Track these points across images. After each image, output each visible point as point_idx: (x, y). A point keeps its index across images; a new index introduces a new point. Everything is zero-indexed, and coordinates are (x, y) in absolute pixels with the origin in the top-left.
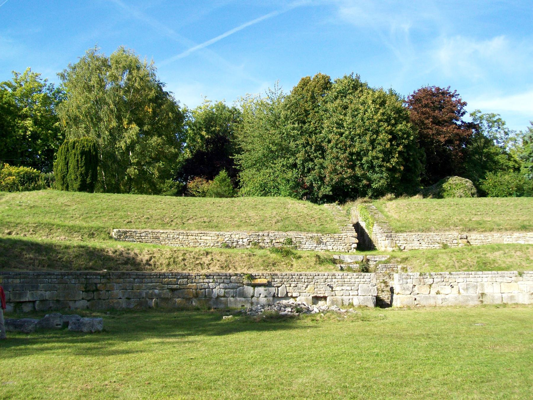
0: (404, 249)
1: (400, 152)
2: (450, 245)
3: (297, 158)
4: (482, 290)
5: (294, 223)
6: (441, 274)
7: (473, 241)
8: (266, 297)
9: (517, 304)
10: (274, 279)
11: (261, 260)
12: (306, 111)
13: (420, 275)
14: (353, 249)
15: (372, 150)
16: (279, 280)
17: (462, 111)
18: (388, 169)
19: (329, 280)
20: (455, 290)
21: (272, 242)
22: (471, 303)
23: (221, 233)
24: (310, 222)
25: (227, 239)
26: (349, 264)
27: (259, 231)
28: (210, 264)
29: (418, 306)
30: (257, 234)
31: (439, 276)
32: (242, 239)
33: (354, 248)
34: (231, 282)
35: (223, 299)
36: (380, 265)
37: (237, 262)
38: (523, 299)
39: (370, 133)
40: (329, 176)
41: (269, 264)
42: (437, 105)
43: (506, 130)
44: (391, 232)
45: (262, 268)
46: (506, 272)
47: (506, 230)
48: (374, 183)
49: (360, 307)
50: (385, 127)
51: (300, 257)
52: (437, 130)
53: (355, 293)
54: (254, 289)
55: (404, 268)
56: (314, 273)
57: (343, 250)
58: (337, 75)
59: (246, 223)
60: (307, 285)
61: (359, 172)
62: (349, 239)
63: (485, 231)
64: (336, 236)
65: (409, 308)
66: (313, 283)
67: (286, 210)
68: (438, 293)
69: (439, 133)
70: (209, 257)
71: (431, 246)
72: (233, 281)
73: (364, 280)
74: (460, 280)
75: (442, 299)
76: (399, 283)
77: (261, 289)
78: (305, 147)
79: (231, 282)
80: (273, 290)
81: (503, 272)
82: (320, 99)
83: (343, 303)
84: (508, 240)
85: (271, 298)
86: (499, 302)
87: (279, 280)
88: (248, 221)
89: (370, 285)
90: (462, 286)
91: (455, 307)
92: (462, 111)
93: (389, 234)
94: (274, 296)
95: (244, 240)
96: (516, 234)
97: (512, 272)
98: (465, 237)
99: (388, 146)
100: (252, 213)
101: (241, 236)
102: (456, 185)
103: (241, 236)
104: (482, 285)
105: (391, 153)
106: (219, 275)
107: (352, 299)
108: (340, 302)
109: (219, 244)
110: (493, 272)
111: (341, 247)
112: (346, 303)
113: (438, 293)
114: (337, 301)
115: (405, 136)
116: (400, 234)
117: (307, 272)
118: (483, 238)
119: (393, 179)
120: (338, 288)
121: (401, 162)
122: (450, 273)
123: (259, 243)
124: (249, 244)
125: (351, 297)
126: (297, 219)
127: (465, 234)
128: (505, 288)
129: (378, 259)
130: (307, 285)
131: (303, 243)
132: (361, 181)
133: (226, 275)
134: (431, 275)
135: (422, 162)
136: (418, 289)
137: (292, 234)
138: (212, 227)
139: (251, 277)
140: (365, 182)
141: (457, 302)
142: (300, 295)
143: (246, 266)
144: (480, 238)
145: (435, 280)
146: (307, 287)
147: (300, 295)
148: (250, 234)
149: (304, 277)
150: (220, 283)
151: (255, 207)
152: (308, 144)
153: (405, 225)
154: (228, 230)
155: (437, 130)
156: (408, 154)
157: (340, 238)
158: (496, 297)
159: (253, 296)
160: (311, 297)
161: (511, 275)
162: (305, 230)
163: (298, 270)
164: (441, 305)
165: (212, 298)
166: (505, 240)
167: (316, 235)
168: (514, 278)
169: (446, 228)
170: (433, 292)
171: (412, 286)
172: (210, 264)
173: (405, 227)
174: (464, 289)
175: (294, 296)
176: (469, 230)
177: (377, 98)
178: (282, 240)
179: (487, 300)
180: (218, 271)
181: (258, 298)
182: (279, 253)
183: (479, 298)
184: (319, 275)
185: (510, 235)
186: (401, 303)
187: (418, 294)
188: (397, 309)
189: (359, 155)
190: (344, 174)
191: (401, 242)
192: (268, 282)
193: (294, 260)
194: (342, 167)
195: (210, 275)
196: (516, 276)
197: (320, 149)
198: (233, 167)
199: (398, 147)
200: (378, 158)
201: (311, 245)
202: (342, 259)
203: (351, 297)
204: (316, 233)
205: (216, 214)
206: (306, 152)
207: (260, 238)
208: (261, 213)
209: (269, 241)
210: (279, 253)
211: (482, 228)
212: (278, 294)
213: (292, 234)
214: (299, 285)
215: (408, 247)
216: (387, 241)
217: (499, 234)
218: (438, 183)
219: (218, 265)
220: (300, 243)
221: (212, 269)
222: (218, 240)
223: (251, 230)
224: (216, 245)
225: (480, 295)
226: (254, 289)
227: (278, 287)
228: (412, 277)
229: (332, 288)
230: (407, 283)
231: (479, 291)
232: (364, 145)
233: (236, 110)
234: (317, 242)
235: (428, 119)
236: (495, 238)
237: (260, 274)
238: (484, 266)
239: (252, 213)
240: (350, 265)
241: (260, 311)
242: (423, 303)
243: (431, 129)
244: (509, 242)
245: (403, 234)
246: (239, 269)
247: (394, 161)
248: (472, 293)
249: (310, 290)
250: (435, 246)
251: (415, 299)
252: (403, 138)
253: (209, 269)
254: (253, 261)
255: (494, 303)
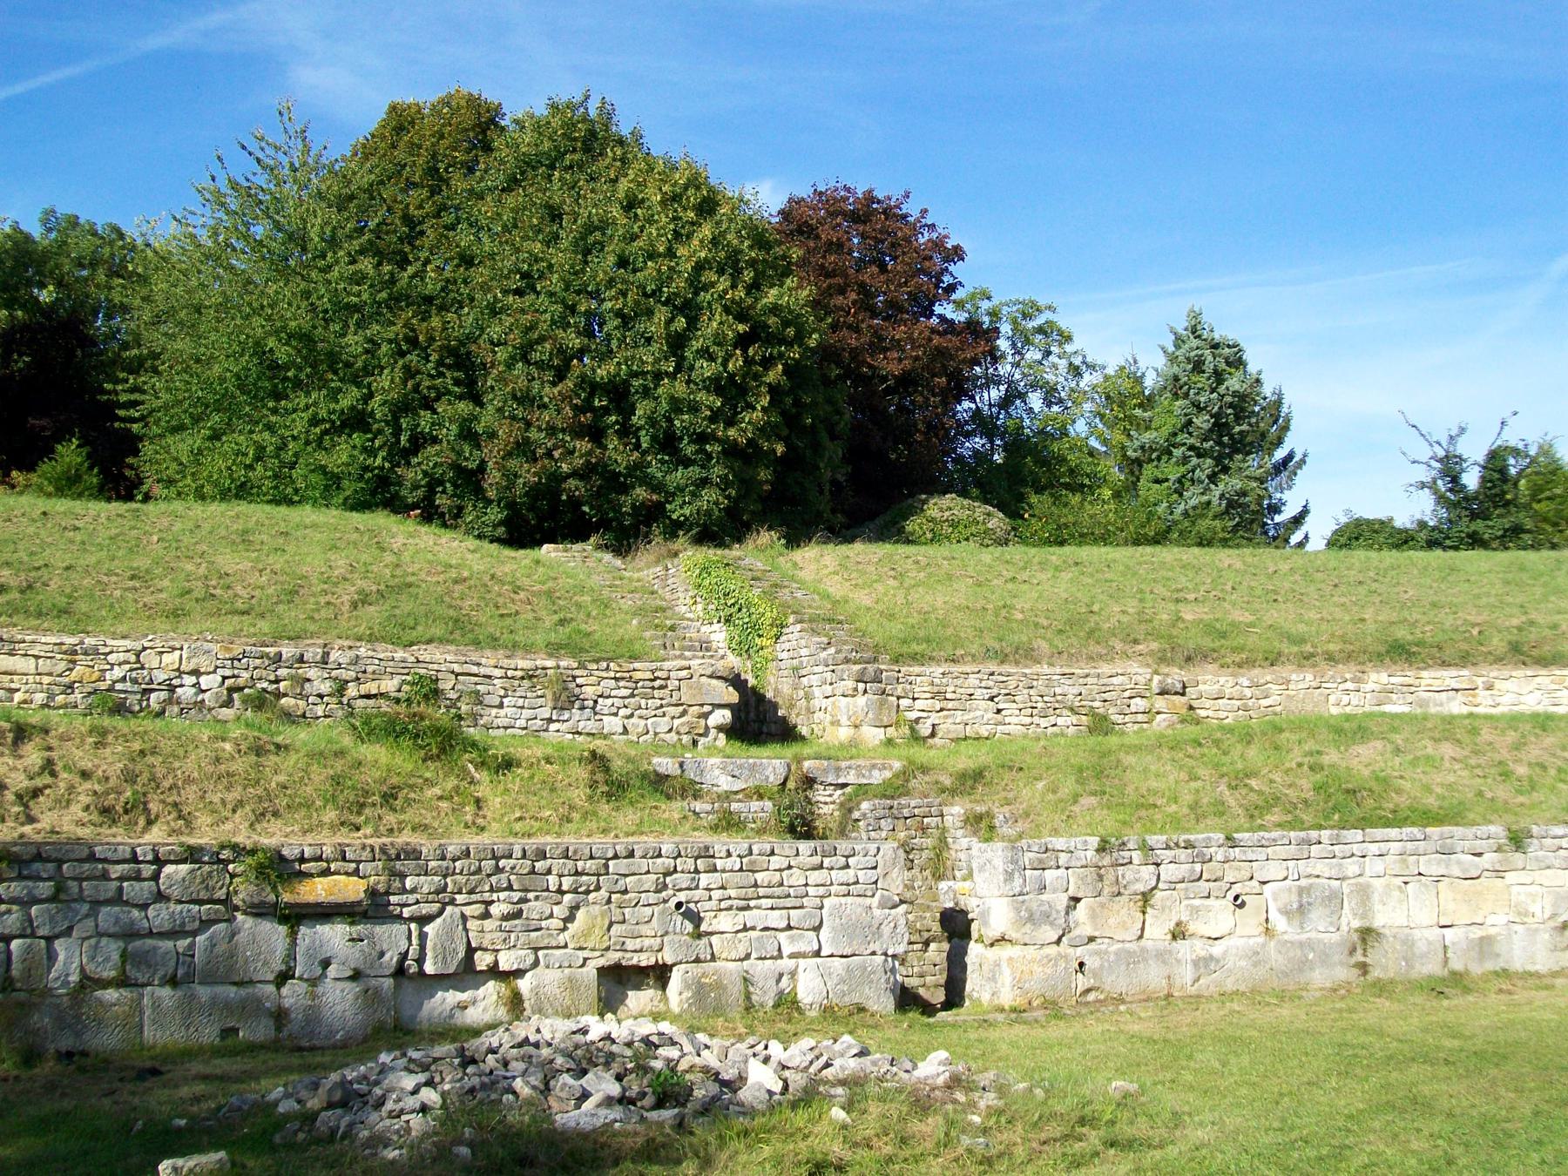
0: (933, 735)
1: (773, 390)
2: (1119, 719)
3: (371, 395)
4: (1364, 916)
5: (440, 610)
6: (1189, 845)
7: (1208, 704)
8: (356, 976)
9: (1505, 973)
10: (403, 876)
11: (319, 774)
12: (407, 219)
13: (1101, 849)
14: (713, 732)
15: (672, 376)
16: (427, 884)
17: (947, 279)
18: (732, 451)
19: (682, 879)
20: (1249, 922)
21: (341, 689)
22: (1319, 978)
23: (90, 641)
24: (514, 608)
25: (118, 672)
26: (728, 796)
27: (276, 639)
28: (36, 793)
29: (1091, 997)
30: (272, 650)
31: (1183, 854)
32: (196, 673)
33: (720, 728)
34: (161, 897)
35: (111, 994)
36: (865, 806)
37: (189, 780)
38: (1530, 951)
39: (662, 314)
40: (501, 467)
41: (366, 793)
42: (867, 254)
43: (1077, 361)
44: (876, 662)
45: (330, 815)
46: (1458, 831)
47: (1331, 658)
48: (679, 501)
49: (828, 1011)
50: (725, 292)
51: (508, 764)
52: (876, 333)
53: (807, 942)
54: (293, 934)
55: (979, 818)
56: (602, 843)
57: (673, 737)
58: (524, 97)
59: (211, 600)
60: (575, 908)
61: (618, 454)
62: (700, 687)
63: (1249, 663)
64: (642, 670)
65: (1052, 1008)
66: (603, 893)
67: (389, 558)
68: (1178, 934)
69: (878, 344)
70: (33, 755)
71: (1044, 723)
72: (175, 892)
73: (849, 875)
74: (1274, 870)
75: (1196, 963)
76: (1006, 889)
77: (334, 935)
78: (402, 354)
79: (161, 897)
80: (393, 939)
81: (1446, 829)
82: (459, 183)
83: (748, 996)
84: (1345, 699)
85: (388, 983)
86: (1431, 967)
87: (427, 884)
88: (218, 592)
89: (875, 901)
90: (1275, 897)
91: (1254, 996)
92: (947, 279)
93: (871, 668)
94: (400, 971)
95: (205, 681)
96: (1378, 678)
97: (1483, 830)
98: (1179, 687)
99: (736, 363)
100: (229, 561)
101: (193, 659)
102: (954, 524)
103: (193, 659)
104: (1364, 893)
105: (743, 391)
106: (92, 857)
107: (793, 974)
108: (736, 990)
109: (77, 696)
110: (1408, 831)
111: (663, 725)
112: (765, 996)
113: (1178, 934)
114: (719, 986)
115: (791, 331)
116: (917, 669)
117: (569, 840)
118: (1248, 693)
119: (747, 485)
120: (725, 922)
121: (776, 426)
122: (1228, 838)
123: (279, 695)
124: (228, 703)
125: (786, 964)
126: (449, 593)
127: (1175, 676)
128: (1452, 902)
129: (851, 778)
130: (575, 908)
131: (487, 700)
132: (625, 489)
133: (134, 859)
134: (1146, 848)
135: (833, 437)
136: (1093, 916)
137: (439, 659)
138: (39, 615)
139: (280, 868)
140: (641, 493)
141: (1261, 972)
142: (536, 963)
143: (240, 804)
144: (1235, 692)
145: (1168, 872)
146: (570, 918)
147: (536, 963)
148: (237, 650)
149: (557, 865)
150: (97, 904)
151: (245, 539)
152: (413, 342)
153: (922, 634)
154: (121, 629)
155: (876, 333)
156: (797, 403)
157: (658, 682)
158: (1421, 947)
159: (283, 977)
160: (590, 971)
161: (1479, 845)
162: (494, 642)
163: (518, 827)
164: (1193, 990)
165: (48, 992)
166: (1332, 699)
167: (550, 663)
168: (1489, 859)
169: (1095, 649)
170: (1157, 930)
171: (1062, 900)
172: (36, 793)
173: (928, 641)
174: (1286, 912)
175: (504, 966)
176: (1189, 659)
177: (686, 187)
178: (389, 685)
179: (1385, 964)
180: (85, 832)
181: (314, 982)
182: (406, 742)
183: (1353, 951)
184: (631, 855)
185: (1355, 680)
186: (1018, 985)
187: (1091, 939)
188: (1000, 1017)
189: (619, 395)
190: (561, 459)
191: (919, 704)
192: (372, 893)
193: (482, 776)
194: (552, 430)
195: (38, 857)
196: (1499, 850)
197: (465, 368)
198: (116, 425)
199: (766, 369)
200: (694, 408)
201: (527, 713)
202: (691, 774)
203: (786, 964)
204: (551, 655)
205: (60, 559)
206: (409, 373)
207: (282, 672)
208: (277, 562)
209: (325, 688)
210: (406, 742)
211: (1234, 650)
212: (420, 960)
213: (438, 657)
214: (534, 908)
215: (949, 726)
216: (861, 700)
217: (1309, 677)
218: (887, 517)
219: (85, 799)
220: (478, 699)
221: (46, 821)
222: (74, 675)
223: (237, 633)
224: (60, 699)
225: (1355, 937)
226: (293, 934)
227: (424, 920)
228: (1063, 858)
229: (696, 919)
230: (1043, 888)
231: (1350, 920)
232: (647, 357)
233: (121, 236)
234: (556, 699)
235: (842, 291)
236: (1293, 691)
237: (328, 851)
238: (1351, 806)
239: (229, 561)
240: (735, 806)
241: (411, 1102)
242: (1117, 982)
243: (857, 330)
244: (1348, 710)
245: (927, 670)
246: (203, 820)
247: (754, 416)
248: (1327, 930)
249: (586, 934)
250: (1060, 721)
251: (1081, 965)
252: (783, 341)
253: (31, 820)
254: (282, 778)
255: (1414, 974)
